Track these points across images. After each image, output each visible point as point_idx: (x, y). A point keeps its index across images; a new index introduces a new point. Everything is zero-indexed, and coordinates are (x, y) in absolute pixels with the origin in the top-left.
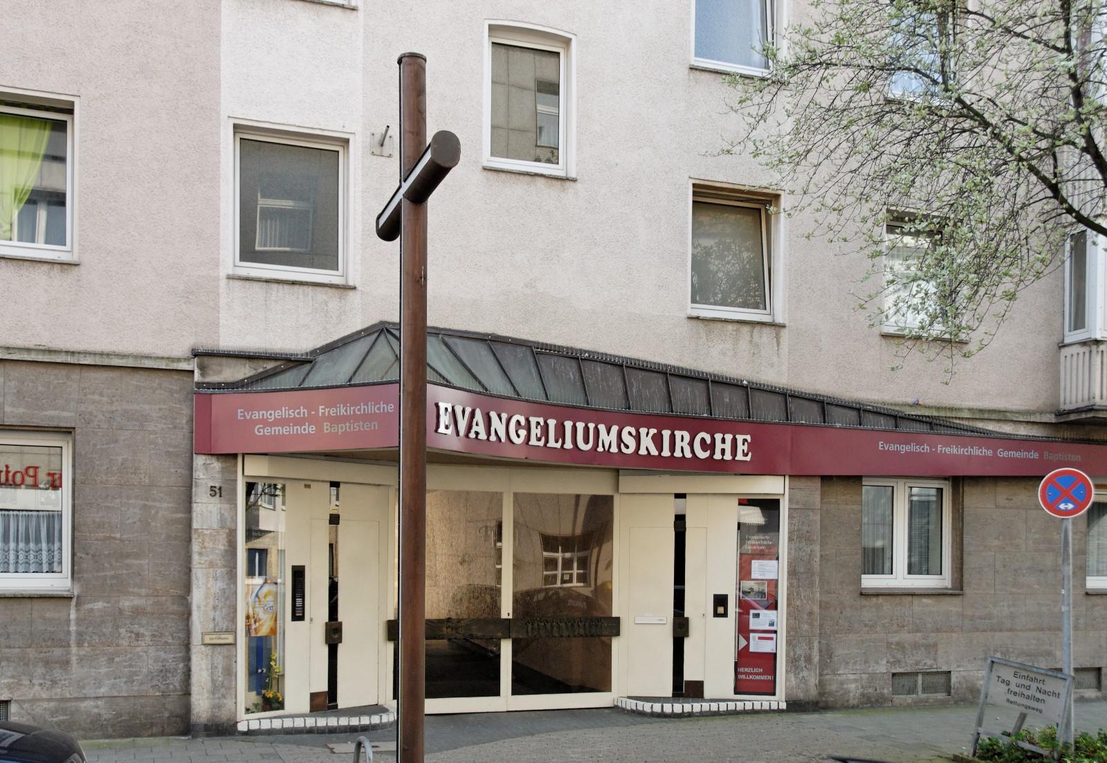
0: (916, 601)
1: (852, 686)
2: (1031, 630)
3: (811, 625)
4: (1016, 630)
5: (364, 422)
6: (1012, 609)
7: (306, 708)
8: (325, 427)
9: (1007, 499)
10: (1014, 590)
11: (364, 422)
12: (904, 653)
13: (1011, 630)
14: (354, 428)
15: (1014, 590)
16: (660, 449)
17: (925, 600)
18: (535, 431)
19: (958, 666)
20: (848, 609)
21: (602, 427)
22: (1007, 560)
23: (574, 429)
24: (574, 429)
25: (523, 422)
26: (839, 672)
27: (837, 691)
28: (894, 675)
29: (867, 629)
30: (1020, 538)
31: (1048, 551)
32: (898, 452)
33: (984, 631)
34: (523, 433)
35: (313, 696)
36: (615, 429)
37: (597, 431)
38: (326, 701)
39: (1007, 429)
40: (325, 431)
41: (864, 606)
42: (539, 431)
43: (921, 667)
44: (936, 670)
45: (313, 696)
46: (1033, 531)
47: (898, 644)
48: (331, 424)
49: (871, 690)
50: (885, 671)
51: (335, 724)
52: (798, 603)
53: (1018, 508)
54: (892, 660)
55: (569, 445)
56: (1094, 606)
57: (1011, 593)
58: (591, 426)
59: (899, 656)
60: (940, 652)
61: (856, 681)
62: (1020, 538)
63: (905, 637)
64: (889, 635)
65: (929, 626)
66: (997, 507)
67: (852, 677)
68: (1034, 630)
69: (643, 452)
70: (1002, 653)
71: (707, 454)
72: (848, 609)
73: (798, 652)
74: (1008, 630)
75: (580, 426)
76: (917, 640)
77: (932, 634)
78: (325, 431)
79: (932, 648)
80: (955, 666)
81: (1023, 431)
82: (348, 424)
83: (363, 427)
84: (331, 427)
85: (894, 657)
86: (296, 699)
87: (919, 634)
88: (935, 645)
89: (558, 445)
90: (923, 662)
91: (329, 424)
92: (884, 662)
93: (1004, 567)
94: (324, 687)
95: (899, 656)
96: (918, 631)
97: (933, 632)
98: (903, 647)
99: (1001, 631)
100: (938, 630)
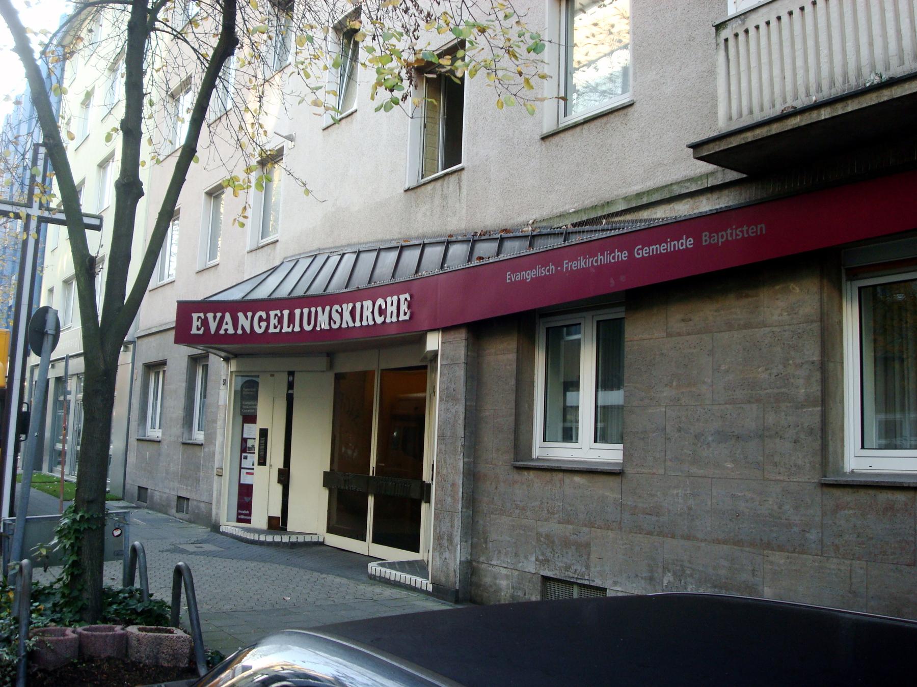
0: (568, 479)
1: (504, 583)
2: (718, 542)
3: (453, 497)
4: (697, 539)
5: (749, 226)
6: (691, 502)
7: (264, 525)
8: (704, 239)
9: (683, 320)
10: (694, 470)
11: (749, 226)
12: (553, 551)
13: (688, 538)
14: (737, 235)
15: (694, 470)
16: (354, 321)
17: (577, 479)
18: (273, 321)
19: (615, 583)
20: (502, 484)
21: (320, 309)
22: (683, 419)
23: (302, 314)
24: (302, 314)
25: (264, 316)
26: (492, 563)
27: (491, 586)
28: (546, 579)
29: (517, 511)
30: (704, 382)
31: (749, 402)
32: (523, 281)
33: (650, 533)
34: (264, 324)
35: (271, 519)
36: (328, 308)
37: (316, 312)
38: (278, 524)
39: (683, 209)
40: (704, 244)
41: (515, 482)
42: (276, 321)
43: (571, 575)
44: (586, 582)
45: (271, 519)
46: (723, 368)
47: (548, 536)
48: (710, 234)
49: (520, 593)
50: (534, 572)
51: (256, 538)
52: (444, 472)
53: (699, 332)
54: (541, 558)
55: (297, 329)
56: (838, 508)
57: (689, 476)
58: (313, 310)
59: (549, 554)
60: (593, 556)
61: (507, 577)
62: (704, 382)
63: (554, 527)
64: (539, 523)
65: (581, 516)
66: (669, 335)
67: (504, 571)
68: (725, 542)
69: (344, 326)
70: (674, 574)
71: (382, 319)
72: (502, 484)
73: (443, 530)
74: (683, 537)
75: (306, 311)
76: (568, 534)
77: (584, 529)
78: (704, 244)
79: (583, 548)
80: (611, 582)
81: (705, 205)
82: (729, 231)
83: (748, 233)
84: (710, 238)
85: (543, 554)
86: (259, 520)
87: (571, 527)
88: (588, 545)
89: (290, 330)
90: (574, 568)
91: (707, 233)
92: (533, 559)
93: (679, 430)
94: (277, 513)
95: (549, 554)
96: (569, 522)
97: (586, 526)
98: (553, 542)
99: (673, 537)
100: (591, 525)
